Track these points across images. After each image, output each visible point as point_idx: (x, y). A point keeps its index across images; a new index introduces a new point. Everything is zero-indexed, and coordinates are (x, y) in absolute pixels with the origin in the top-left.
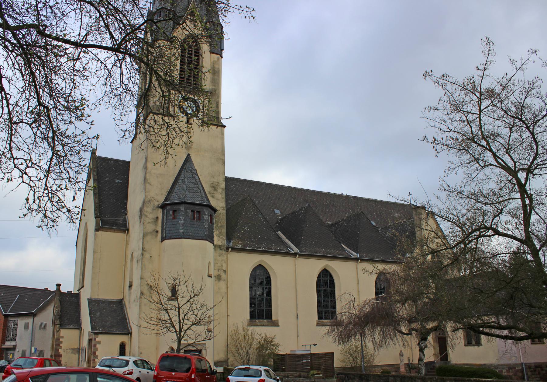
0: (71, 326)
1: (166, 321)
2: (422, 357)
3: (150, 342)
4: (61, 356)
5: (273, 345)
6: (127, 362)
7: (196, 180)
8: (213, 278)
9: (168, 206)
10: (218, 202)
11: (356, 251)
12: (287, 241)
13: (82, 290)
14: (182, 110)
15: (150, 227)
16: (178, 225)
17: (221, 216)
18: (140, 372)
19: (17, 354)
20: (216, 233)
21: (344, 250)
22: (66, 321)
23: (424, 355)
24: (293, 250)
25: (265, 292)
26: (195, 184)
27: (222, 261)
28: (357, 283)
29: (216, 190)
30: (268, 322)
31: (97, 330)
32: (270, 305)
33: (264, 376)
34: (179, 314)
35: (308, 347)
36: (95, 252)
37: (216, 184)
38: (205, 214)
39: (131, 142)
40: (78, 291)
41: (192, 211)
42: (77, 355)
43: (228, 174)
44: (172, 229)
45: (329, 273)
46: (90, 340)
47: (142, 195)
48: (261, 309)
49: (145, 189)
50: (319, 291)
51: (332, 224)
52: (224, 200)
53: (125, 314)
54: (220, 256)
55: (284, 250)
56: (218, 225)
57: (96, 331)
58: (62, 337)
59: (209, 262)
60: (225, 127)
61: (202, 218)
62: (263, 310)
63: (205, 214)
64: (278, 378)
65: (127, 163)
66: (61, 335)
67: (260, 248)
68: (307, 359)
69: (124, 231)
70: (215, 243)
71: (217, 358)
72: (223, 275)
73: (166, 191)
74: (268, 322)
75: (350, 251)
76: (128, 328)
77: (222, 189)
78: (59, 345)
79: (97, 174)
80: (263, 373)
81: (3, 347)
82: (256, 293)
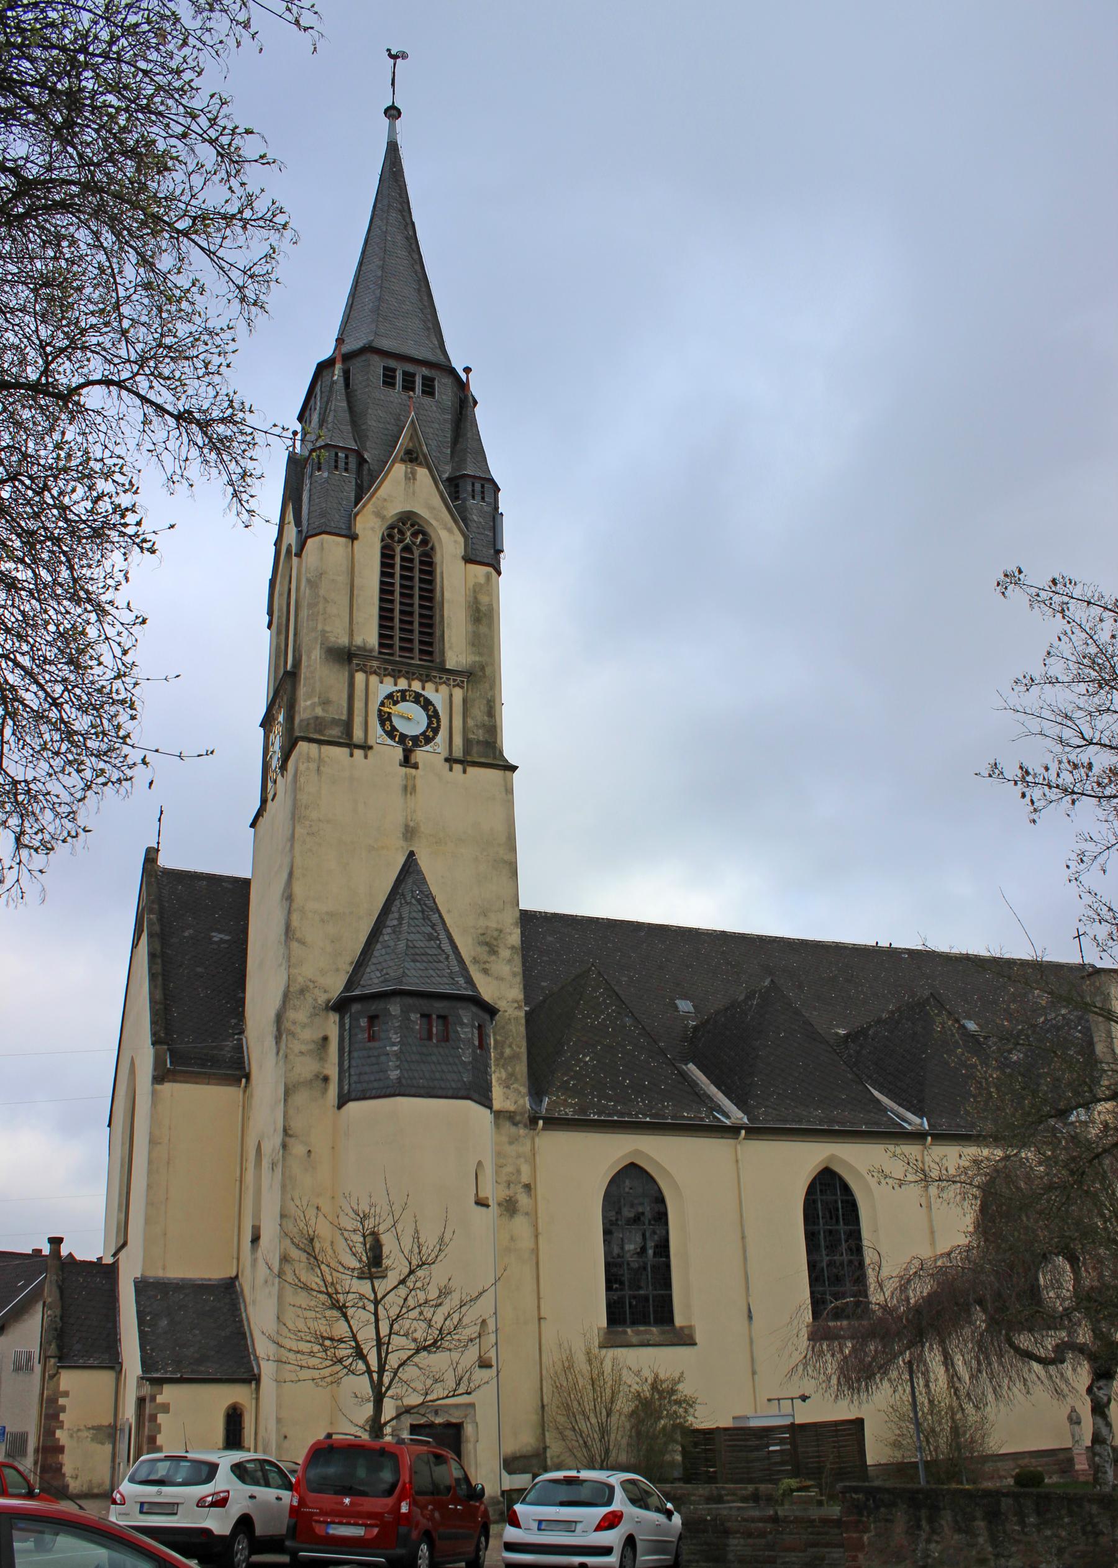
1: (341, 1341)
2: (1104, 1431)
3: (303, 1406)
4: (61, 1450)
5: (678, 1403)
6: (212, 1470)
7: (433, 926)
9: (357, 1005)
10: (502, 986)
11: (919, 1113)
12: (713, 1090)
13: (122, 1255)
15: (306, 1067)
18: (252, 1497)
20: (496, 1077)
21: (884, 1109)
22: (77, 1347)
23: (1109, 1425)
24: (728, 1117)
25: (650, 1244)
26: (430, 938)
27: (519, 1156)
28: (919, 1211)
29: (493, 951)
31: (157, 1371)
32: (667, 1283)
34: (377, 1321)
35: (786, 1405)
36: (153, 1142)
37: (495, 934)
38: (462, 1024)
39: (253, 825)
40: (114, 1255)
41: (423, 1016)
42: (108, 1447)
43: (529, 902)
44: (367, 1069)
45: (841, 1179)
46: (141, 1401)
47: (286, 973)
48: (640, 1297)
49: (289, 958)
50: (813, 1234)
51: (847, 1036)
52: (519, 979)
53: (241, 1321)
54: (511, 1143)
55: (702, 1119)
56: (502, 1054)
57: (155, 1375)
58: (66, 1394)
59: (480, 1163)
60: (514, 768)
61: (452, 1035)
62: (646, 1298)
63: (462, 1024)
64: (669, 1506)
65: (243, 885)
66: (62, 1388)
67: (630, 1115)
68: (782, 1441)
70: (497, 1105)
71: (511, 1447)
72: (523, 1200)
73: (349, 959)
74: (663, 1333)
75: (901, 1110)
76: (250, 1362)
77: (513, 947)
78: (56, 1417)
79: (161, 919)
80: (619, 1494)
82: (622, 1248)
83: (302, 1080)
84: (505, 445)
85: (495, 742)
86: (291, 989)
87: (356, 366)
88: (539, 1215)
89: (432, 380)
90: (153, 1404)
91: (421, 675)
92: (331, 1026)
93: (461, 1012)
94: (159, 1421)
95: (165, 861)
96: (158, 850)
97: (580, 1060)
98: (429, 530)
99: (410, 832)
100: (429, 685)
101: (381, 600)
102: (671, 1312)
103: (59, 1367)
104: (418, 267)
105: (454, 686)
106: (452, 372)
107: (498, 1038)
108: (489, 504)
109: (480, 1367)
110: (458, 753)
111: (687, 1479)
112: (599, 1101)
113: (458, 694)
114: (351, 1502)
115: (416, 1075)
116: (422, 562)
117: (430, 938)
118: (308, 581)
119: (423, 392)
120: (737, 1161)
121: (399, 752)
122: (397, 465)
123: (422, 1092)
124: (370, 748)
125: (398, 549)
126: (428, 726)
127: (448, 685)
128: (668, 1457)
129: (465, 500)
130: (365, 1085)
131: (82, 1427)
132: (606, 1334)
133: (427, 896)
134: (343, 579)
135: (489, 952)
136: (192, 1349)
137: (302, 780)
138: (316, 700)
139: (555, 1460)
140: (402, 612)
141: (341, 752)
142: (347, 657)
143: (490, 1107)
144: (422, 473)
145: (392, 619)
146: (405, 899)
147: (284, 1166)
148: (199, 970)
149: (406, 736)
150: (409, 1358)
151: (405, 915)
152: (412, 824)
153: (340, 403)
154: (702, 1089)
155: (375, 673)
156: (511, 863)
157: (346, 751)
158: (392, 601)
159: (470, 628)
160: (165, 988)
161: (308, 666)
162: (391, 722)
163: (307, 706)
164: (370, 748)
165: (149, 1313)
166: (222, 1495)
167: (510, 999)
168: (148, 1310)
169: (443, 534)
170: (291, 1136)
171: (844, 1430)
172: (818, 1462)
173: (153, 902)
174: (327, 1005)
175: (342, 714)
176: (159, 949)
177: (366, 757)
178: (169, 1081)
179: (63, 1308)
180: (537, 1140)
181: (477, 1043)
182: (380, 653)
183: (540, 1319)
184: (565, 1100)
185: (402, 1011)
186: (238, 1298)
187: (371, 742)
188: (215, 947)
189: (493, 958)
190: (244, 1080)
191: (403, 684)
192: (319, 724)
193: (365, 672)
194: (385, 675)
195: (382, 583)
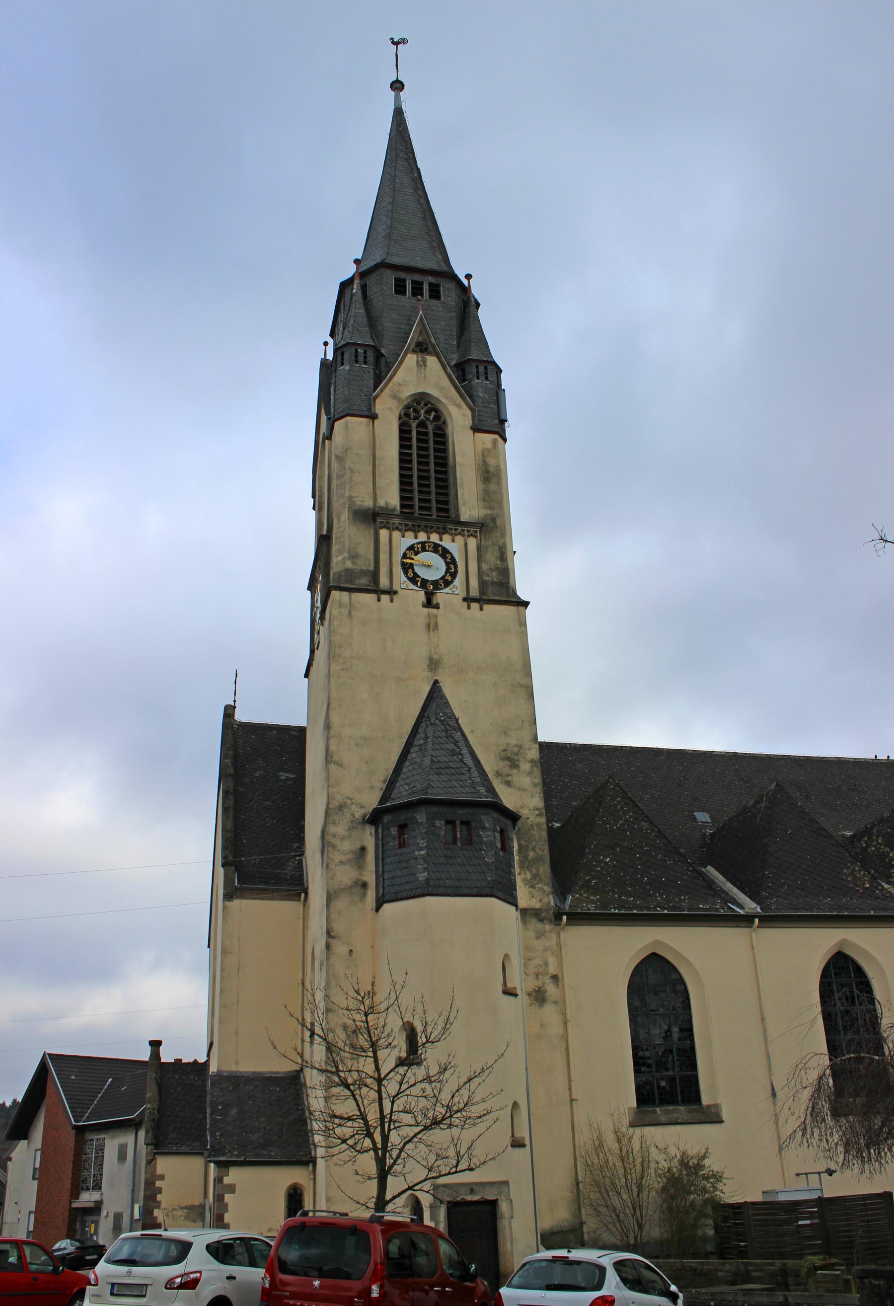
0: (183, 1149)
5: (706, 1178)
6: (185, 1248)
7: (456, 743)
8: (522, 998)
9: (390, 816)
10: (523, 796)
12: (729, 886)
14: (411, 574)
15: (346, 875)
16: (412, 862)
17: (535, 832)
19: (105, 1224)
24: (742, 907)
26: (453, 753)
27: (545, 950)
30: (690, 1111)
31: (224, 1154)
33: (612, 1285)
37: (516, 749)
41: (447, 822)
44: (399, 873)
48: (668, 1078)
49: (328, 778)
52: (539, 789)
54: (538, 938)
55: (717, 910)
56: (526, 857)
58: (162, 1177)
59: (506, 956)
60: (526, 604)
64: (673, 1288)
65: (302, 731)
66: (159, 1171)
67: (649, 908)
68: (811, 1216)
69: (297, 897)
70: (523, 902)
71: (547, 1223)
72: (551, 990)
73: (382, 778)
77: (532, 761)
81: (75, 1205)
83: (342, 886)
84: (501, 332)
85: (508, 582)
86: (331, 806)
87: (372, 280)
88: (568, 1003)
89: (438, 286)
90: (220, 1185)
91: (438, 528)
92: (368, 838)
93: (482, 817)
94: (226, 1201)
95: (241, 716)
96: (235, 707)
97: (602, 861)
98: (441, 408)
99: (434, 664)
100: (446, 537)
101: (401, 468)
102: (698, 1091)
103: (155, 1154)
104: (423, 201)
105: (468, 536)
106: (454, 278)
107: (522, 842)
108: (492, 382)
109: (513, 1146)
110: (474, 592)
111: (722, 1254)
112: (620, 897)
113: (472, 543)
114: (321, 1286)
115: (443, 876)
116: (435, 435)
117: (453, 753)
118: (337, 457)
119: (431, 297)
120: (753, 948)
121: (421, 596)
122: (409, 356)
123: (449, 891)
124: (396, 593)
125: (414, 425)
126: (447, 571)
127: (463, 536)
128: (700, 1232)
129: (470, 381)
130: (397, 887)
131: (177, 1207)
132: (636, 1113)
133: (450, 718)
134: (366, 452)
135: (511, 766)
136: (257, 1135)
137: (336, 623)
138: (346, 555)
139: (592, 1235)
140: (419, 477)
141: (370, 598)
142: (373, 517)
143: (516, 906)
144: (432, 360)
145: (411, 484)
146: (429, 720)
147: (327, 964)
148: (267, 803)
149: (427, 581)
150: (415, 1135)
151: (430, 734)
152: (435, 657)
153: (358, 310)
154: (719, 886)
155: (397, 529)
156: (527, 687)
157: (374, 596)
158: (411, 469)
159: (481, 487)
160: (236, 819)
161: (339, 527)
162: (413, 570)
163: (339, 561)
164: (396, 593)
165: (221, 1103)
166: (192, 1276)
167: (532, 808)
168: (220, 1100)
169: (453, 410)
170: (333, 937)
171: (873, 1204)
172: (849, 1237)
173: (229, 749)
174: (364, 819)
175: (369, 566)
176: (232, 787)
177: (392, 601)
178: (237, 898)
179: (160, 1101)
180: (562, 934)
181: (499, 846)
182: (402, 512)
183: (572, 1100)
184: (588, 897)
185: (428, 818)
186: (301, 1089)
187: (396, 587)
188: (282, 784)
189: (515, 771)
190: (303, 895)
191: (422, 537)
192: (350, 574)
193: (388, 528)
194: (406, 530)
195: (401, 454)
